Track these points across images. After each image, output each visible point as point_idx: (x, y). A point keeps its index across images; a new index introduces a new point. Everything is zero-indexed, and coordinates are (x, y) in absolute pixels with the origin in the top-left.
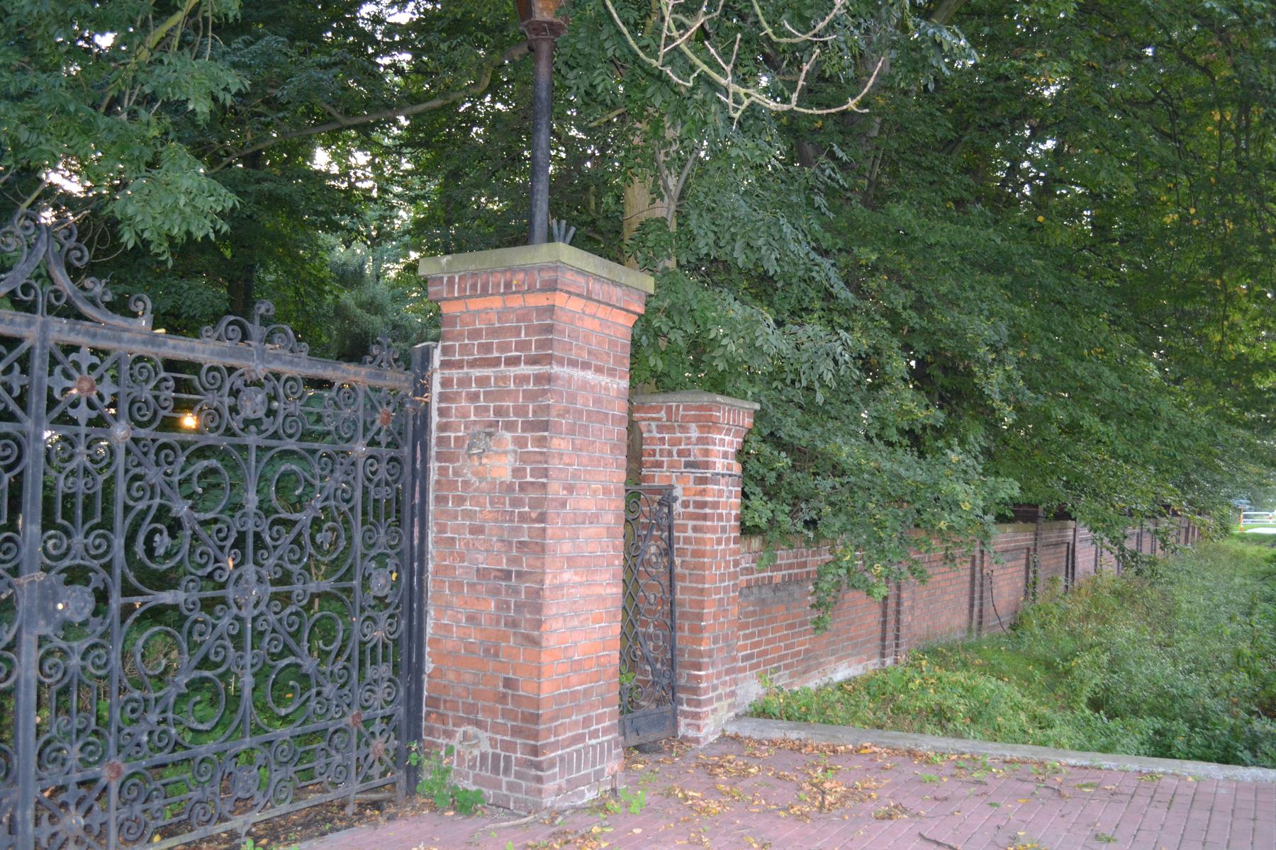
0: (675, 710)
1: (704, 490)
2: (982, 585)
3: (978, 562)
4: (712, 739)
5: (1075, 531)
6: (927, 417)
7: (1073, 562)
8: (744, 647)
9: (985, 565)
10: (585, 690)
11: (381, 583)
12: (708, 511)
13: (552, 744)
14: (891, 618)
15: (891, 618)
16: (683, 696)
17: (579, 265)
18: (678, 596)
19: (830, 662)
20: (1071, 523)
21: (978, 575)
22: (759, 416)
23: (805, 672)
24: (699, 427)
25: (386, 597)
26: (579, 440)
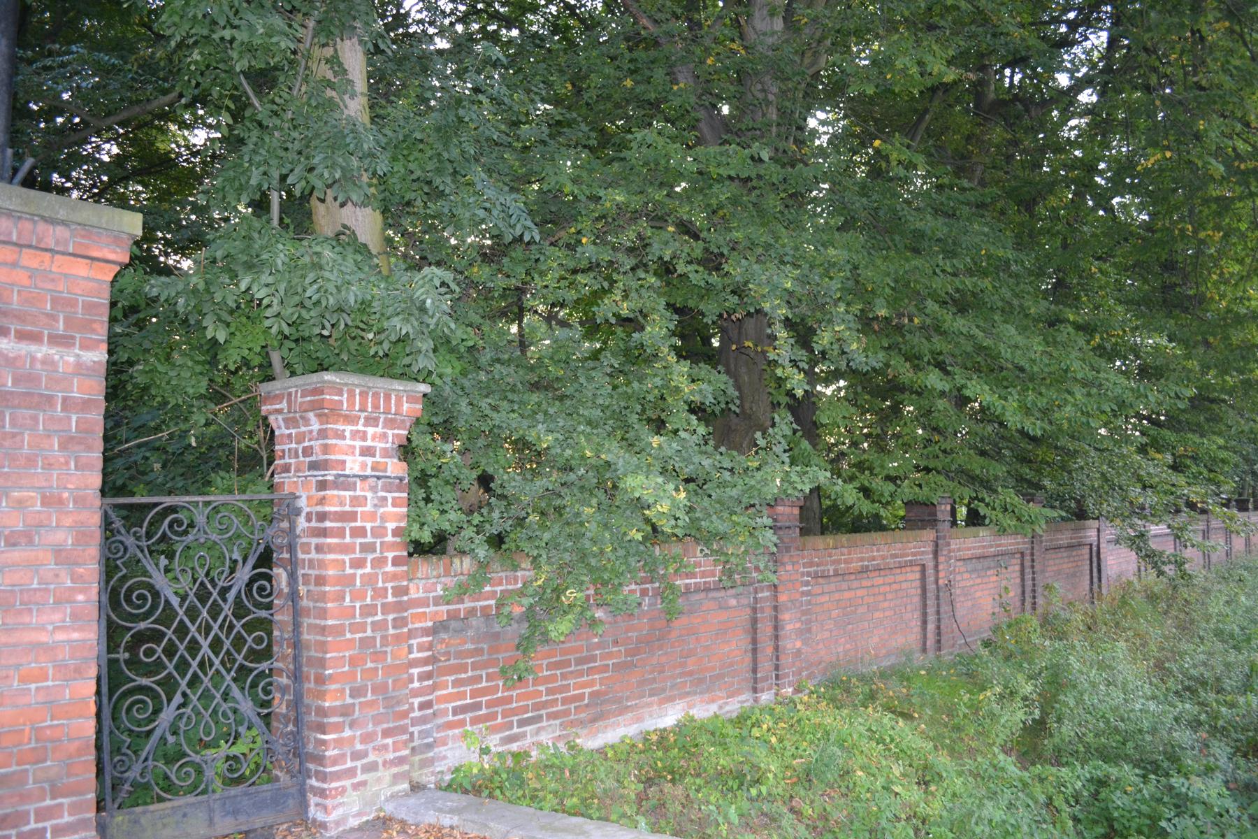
1: (324, 498)
2: (938, 598)
3: (930, 571)
4: (354, 822)
5: (1099, 530)
6: (692, 392)
9: (941, 574)
12: (328, 524)
14: (767, 648)
15: (767, 648)
16: (311, 766)
18: (305, 636)
19: (649, 705)
20: (1093, 524)
21: (931, 587)
23: (594, 720)
24: (318, 416)
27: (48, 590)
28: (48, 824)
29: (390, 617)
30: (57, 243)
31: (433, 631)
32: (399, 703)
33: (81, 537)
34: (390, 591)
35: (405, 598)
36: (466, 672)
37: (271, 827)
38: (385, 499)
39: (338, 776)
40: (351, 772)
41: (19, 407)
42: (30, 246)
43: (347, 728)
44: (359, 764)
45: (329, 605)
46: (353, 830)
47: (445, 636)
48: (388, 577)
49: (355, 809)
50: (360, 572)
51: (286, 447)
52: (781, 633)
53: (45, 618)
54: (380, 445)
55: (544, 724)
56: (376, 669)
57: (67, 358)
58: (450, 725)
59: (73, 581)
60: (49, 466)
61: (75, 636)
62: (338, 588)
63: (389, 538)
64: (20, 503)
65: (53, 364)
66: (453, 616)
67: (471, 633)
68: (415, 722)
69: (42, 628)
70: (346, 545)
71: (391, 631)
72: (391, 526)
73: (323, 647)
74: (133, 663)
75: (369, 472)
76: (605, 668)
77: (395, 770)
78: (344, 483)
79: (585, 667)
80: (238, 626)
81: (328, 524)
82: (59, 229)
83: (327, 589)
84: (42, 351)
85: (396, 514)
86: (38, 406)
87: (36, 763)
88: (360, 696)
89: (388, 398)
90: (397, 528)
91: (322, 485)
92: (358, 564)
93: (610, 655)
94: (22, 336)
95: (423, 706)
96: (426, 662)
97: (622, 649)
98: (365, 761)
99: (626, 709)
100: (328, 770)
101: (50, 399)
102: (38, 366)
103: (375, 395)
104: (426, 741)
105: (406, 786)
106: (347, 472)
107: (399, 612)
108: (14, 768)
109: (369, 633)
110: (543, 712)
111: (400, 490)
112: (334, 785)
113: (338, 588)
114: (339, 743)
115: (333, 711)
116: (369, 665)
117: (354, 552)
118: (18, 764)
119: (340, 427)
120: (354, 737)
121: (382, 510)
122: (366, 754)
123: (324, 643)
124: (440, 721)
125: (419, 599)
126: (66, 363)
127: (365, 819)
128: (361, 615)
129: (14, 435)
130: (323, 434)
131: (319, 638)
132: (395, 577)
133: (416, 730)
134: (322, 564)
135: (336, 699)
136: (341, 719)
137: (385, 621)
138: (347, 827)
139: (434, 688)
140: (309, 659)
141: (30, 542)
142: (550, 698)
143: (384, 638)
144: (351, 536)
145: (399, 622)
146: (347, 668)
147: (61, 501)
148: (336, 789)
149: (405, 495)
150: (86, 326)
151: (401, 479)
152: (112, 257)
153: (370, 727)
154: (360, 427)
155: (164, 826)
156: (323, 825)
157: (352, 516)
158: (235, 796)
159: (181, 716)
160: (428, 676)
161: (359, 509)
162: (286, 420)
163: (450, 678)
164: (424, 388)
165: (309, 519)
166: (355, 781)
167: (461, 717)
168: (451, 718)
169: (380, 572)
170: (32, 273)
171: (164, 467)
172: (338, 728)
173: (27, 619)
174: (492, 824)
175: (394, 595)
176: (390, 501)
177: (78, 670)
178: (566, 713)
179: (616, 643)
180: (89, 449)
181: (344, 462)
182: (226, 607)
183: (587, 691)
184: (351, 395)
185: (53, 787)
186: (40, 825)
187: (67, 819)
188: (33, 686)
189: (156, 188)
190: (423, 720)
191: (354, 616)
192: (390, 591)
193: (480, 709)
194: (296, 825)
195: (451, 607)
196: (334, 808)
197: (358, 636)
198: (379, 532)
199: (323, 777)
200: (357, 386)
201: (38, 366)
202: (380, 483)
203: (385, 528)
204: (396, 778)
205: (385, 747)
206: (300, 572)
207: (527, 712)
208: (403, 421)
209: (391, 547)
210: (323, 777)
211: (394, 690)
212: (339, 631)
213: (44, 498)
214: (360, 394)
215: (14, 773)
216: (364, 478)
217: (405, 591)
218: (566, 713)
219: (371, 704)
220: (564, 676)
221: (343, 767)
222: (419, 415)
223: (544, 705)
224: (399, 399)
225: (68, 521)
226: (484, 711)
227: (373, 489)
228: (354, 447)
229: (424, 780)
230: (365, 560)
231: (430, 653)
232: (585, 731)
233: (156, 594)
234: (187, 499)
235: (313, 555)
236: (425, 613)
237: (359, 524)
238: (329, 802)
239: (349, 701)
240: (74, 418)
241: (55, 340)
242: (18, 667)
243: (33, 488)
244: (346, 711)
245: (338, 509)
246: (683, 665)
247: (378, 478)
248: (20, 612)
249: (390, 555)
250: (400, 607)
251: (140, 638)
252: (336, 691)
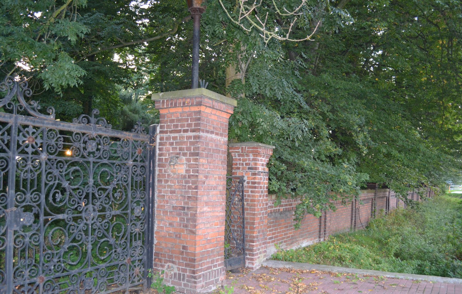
0: (244, 257)
1: (255, 178)
2: (355, 212)
3: (354, 204)
4: (258, 268)
6: (336, 151)
7: (389, 204)
8: (269, 235)
9: (357, 205)
10: (212, 250)
11: (138, 211)
12: (256, 185)
13: (200, 269)
14: (323, 226)
15: (323, 226)
16: (247, 252)
17: (210, 96)
18: (246, 216)
19: (300, 240)
20: (388, 190)
21: (354, 208)
22: (275, 151)
23: (291, 244)
25: (140, 216)
26: (210, 159)
52: (326, 221)
67: (272, 217)
92: (260, 196)
94: (217, 134)
189: (424, 127)
235: (250, 193)
246: (307, 229)
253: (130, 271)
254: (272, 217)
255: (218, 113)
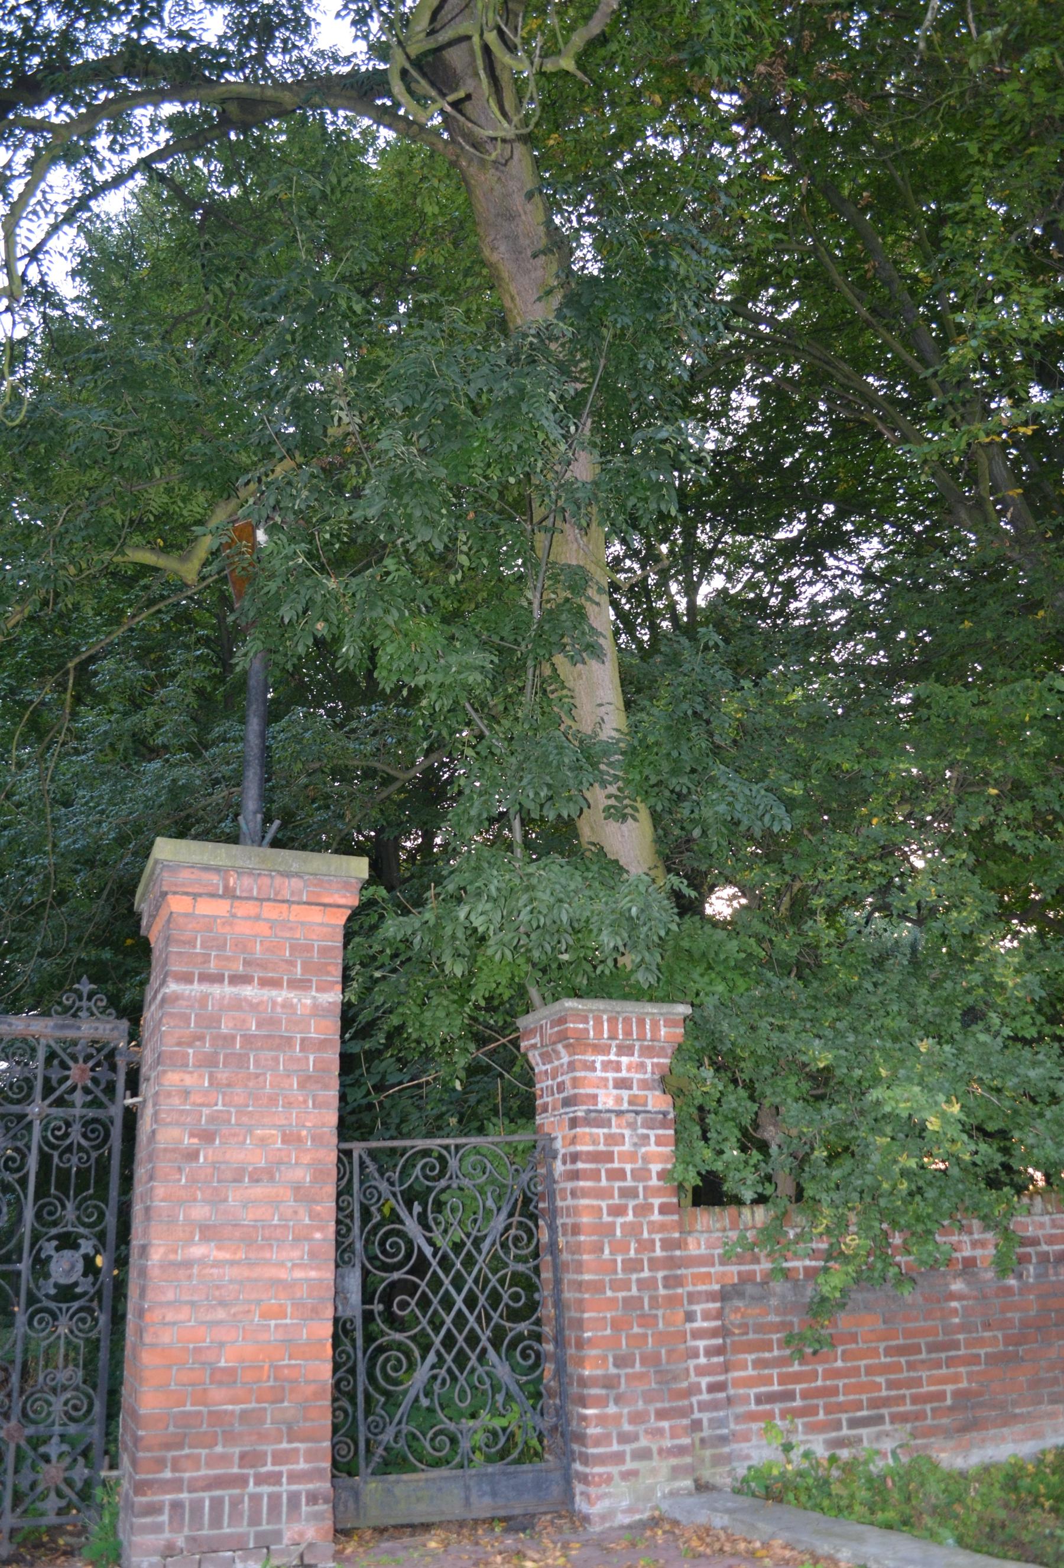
8: (738, 1383)
10: (244, 1412)
12: (580, 1165)
13: (167, 1482)
16: (576, 1447)
17: (196, 858)
22: (694, 1025)
23: (964, 1429)
24: (566, 1047)
27: (286, 1226)
28: (284, 1468)
29: (660, 1275)
30: (293, 894)
31: (723, 1296)
32: (675, 1379)
33: (318, 1176)
34: (658, 1244)
35: (678, 1253)
36: (771, 1350)
37: (533, 1516)
38: (647, 1137)
39: (602, 1460)
40: (618, 1458)
41: (262, 1048)
42: (268, 900)
43: (611, 1403)
44: (628, 1448)
45: (585, 1257)
46: (622, 1527)
47: (740, 1304)
48: (653, 1227)
49: (625, 1504)
50: (620, 1220)
51: (544, 1085)
53: (284, 1255)
54: (637, 1076)
55: (887, 1427)
56: (646, 1336)
57: (304, 1001)
58: (752, 1417)
59: (311, 1218)
60: (289, 1104)
61: (313, 1274)
62: (595, 1238)
63: (654, 1182)
64: (263, 1141)
65: (292, 1007)
66: (746, 1278)
67: (774, 1302)
68: (703, 1407)
69: (281, 1264)
70: (603, 1189)
71: (662, 1291)
72: (655, 1168)
73: (580, 1305)
74: (392, 1320)
75: (625, 1106)
76: (974, 1360)
77: (674, 1461)
78: (597, 1119)
79: (943, 1355)
80: (494, 1281)
81: (580, 1165)
82: (294, 880)
83: (582, 1238)
84: (281, 995)
85: (660, 1154)
86: (279, 1048)
87: (274, 1402)
88: (626, 1366)
89: (641, 1022)
90: (664, 1171)
91: (574, 1123)
92: (618, 1211)
93: (981, 1342)
94: (264, 983)
95: (712, 1388)
96: (714, 1333)
97: (1000, 1335)
98: (635, 1445)
99: (1015, 1419)
100: (592, 1451)
101: (289, 1041)
102: (279, 1009)
103: (627, 1021)
104: (719, 1432)
105: (688, 1483)
106: (600, 1107)
107: (670, 1268)
108: (254, 1405)
109: (634, 1291)
110: (885, 1411)
111: (664, 1125)
112: (597, 1470)
113: (595, 1238)
114: (602, 1420)
115: (594, 1381)
116: (636, 1330)
117: (612, 1197)
118: (258, 1401)
119: (591, 1058)
120: (621, 1415)
121: (644, 1149)
122: (635, 1438)
123: (581, 1301)
124: (740, 1409)
125: (700, 1256)
126: (304, 1005)
127: (637, 1517)
128: (624, 1270)
129: (257, 1076)
130: (572, 1066)
131: (578, 1295)
132: (662, 1227)
133: (705, 1417)
134: (575, 1211)
135: (598, 1367)
136: (603, 1392)
137: (655, 1279)
138: (616, 1524)
139: (726, 1368)
140: (570, 1319)
141: (272, 1178)
142: (893, 1393)
143: (653, 1299)
144: (608, 1179)
145: (671, 1282)
146: (608, 1332)
147: (299, 1139)
148: (600, 1475)
149: (672, 1132)
150: (321, 969)
151: (665, 1114)
152: (342, 901)
153: (641, 1405)
154: (613, 1057)
155: (418, 1500)
156: (586, 1519)
157: (609, 1157)
158: (493, 1474)
159: (434, 1378)
160: (719, 1351)
161: (616, 1149)
162: (541, 1055)
163: (750, 1357)
164: (684, 1009)
165: (564, 1163)
166: (624, 1468)
167: (768, 1407)
168: (753, 1407)
169: (644, 1221)
170: (272, 924)
171: (460, 1121)
172: (601, 1402)
173: (267, 1255)
174: (760, 1525)
175: (663, 1248)
176: (653, 1139)
177: (315, 1310)
178: (919, 1416)
179: (987, 1326)
180: (326, 1087)
181: (595, 1097)
182: (480, 1259)
183: (949, 1388)
184: (598, 1022)
185: (290, 1429)
186: (277, 1468)
187: (302, 1465)
188: (273, 1323)
190: (713, 1406)
191: (615, 1272)
192: (658, 1244)
193: (794, 1399)
194: (560, 1517)
195: (744, 1268)
196: (599, 1498)
197: (621, 1294)
198: (641, 1174)
199: (585, 1460)
200: (604, 1011)
201: (279, 1009)
202: (639, 1119)
203: (649, 1171)
204: (676, 1472)
205: (660, 1432)
206: (559, 1221)
207: (861, 1409)
208: (663, 1048)
209: (657, 1192)
210: (585, 1460)
211: (668, 1362)
212: (598, 1287)
213: (284, 1135)
214: (609, 1020)
215: (253, 1410)
216: (619, 1113)
217: (680, 1244)
218: (919, 1416)
219: (641, 1377)
220: (911, 1366)
221: (608, 1450)
222: (681, 1040)
223: (886, 1402)
224: (655, 1025)
225: (306, 1159)
226: (798, 1403)
227: (632, 1126)
228: (606, 1079)
229: (718, 1481)
230: (626, 1207)
231: (718, 1323)
232: (951, 1443)
233: (410, 1243)
234: (439, 1141)
235: (570, 1202)
236: (709, 1274)
237: (616, 1165)
238: (593, 1491)
239: (613, 1370)
240: (311, 1058)
241: (294, 984)
242: (258, 1302)
243: (274, 1126)
244: (609, 1383)
245: (590, 1148)
247: (637, 1113)
248: (261, 1248)
249: (656, 1202)
250: (671, 1263)
251: (394, 1288)
252: (597, 1357)
253: (16, 1471)
254: (774, 1302)
255: (270, 911)
